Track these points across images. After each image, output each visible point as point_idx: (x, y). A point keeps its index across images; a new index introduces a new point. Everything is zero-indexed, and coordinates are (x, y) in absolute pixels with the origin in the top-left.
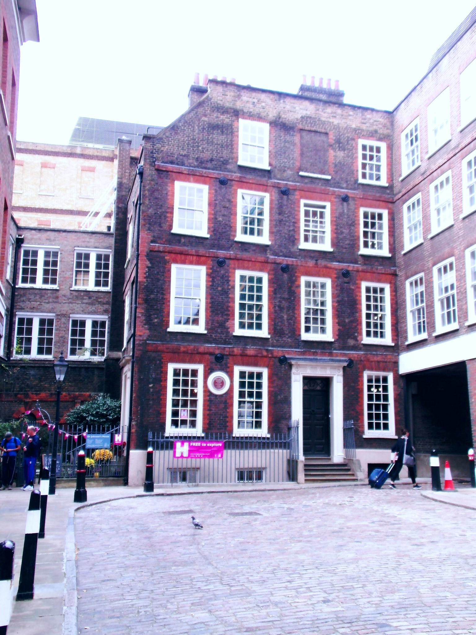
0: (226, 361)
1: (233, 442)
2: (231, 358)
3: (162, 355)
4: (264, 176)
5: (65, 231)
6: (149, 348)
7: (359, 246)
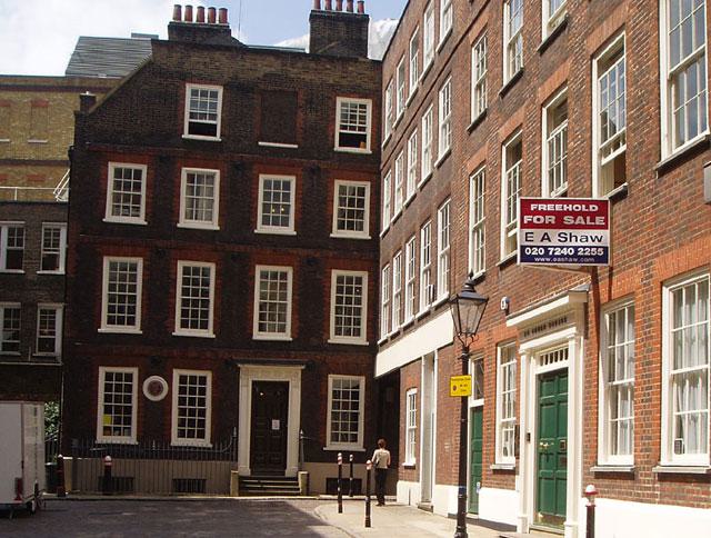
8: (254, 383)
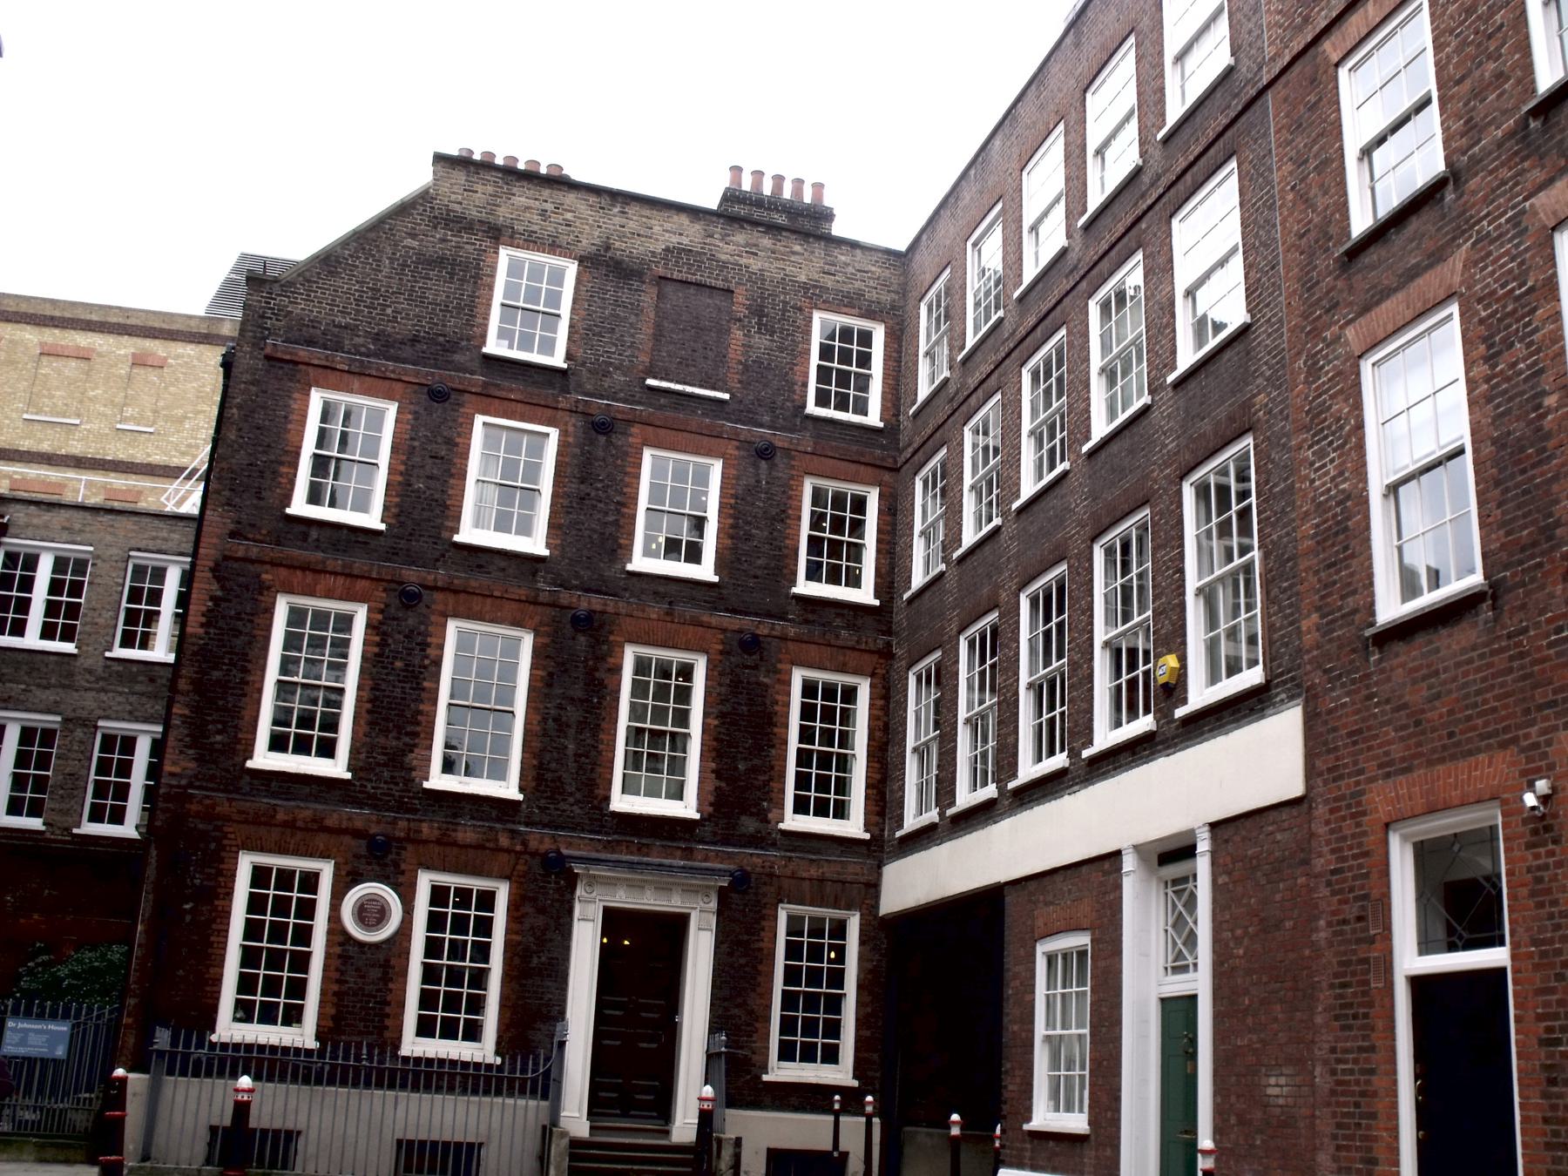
0: (398, 854)
1: (405, 1073)
2: (410, 847)
4: (551, 385)
7: (795, 573)
8: (607, 910)
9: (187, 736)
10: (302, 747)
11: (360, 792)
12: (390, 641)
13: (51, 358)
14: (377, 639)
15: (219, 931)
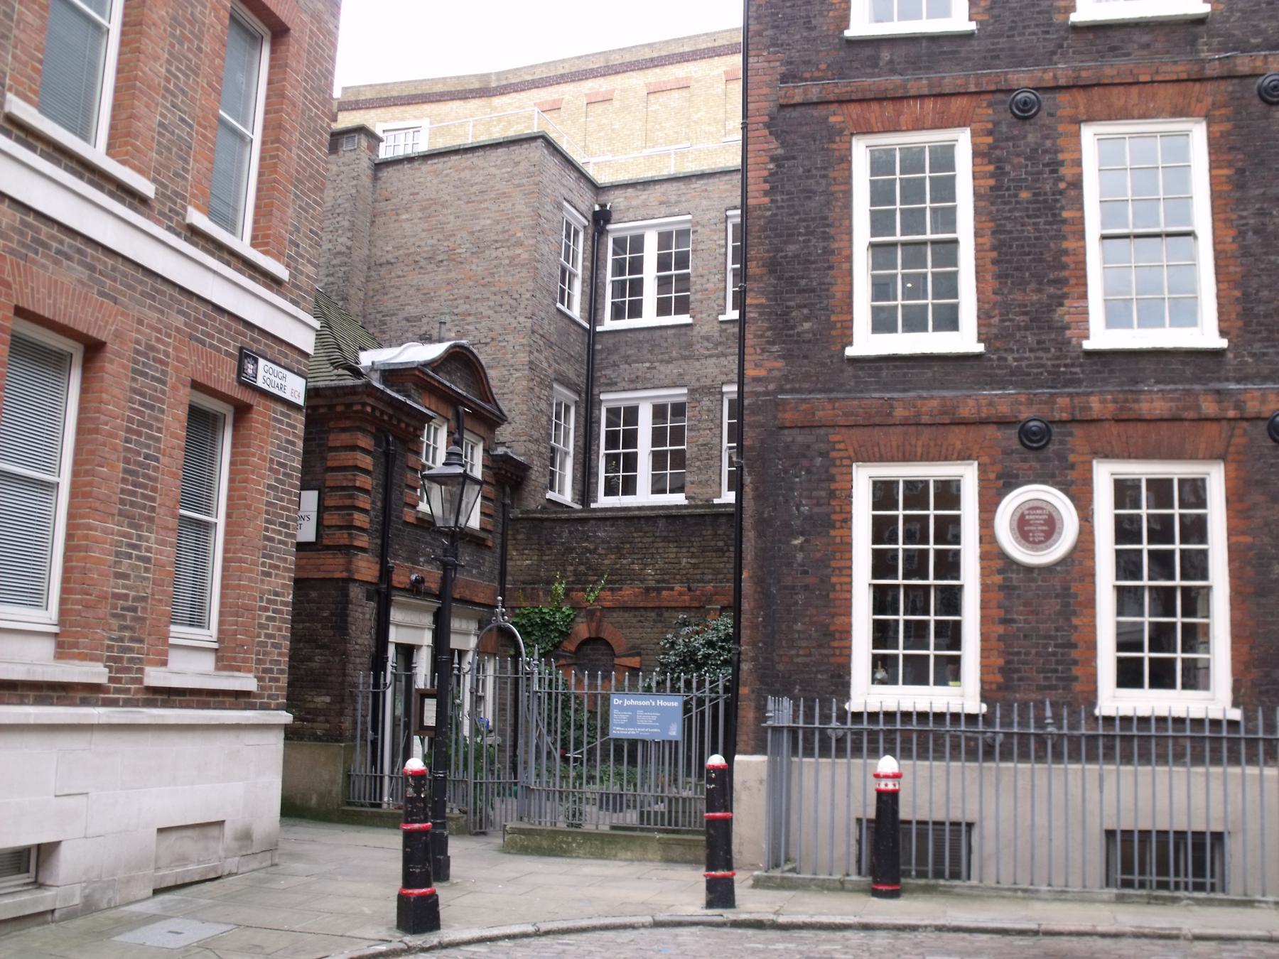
2: (1077, 430)
3: (832, 438)
5: (702, 176)
6: (788, 417)
9: (768, 329)
10: (915, 323)
11: (999, 367)
12: (1008, 168)
13: (657, 95)
14: (991, 168)
15: (840, 569)
